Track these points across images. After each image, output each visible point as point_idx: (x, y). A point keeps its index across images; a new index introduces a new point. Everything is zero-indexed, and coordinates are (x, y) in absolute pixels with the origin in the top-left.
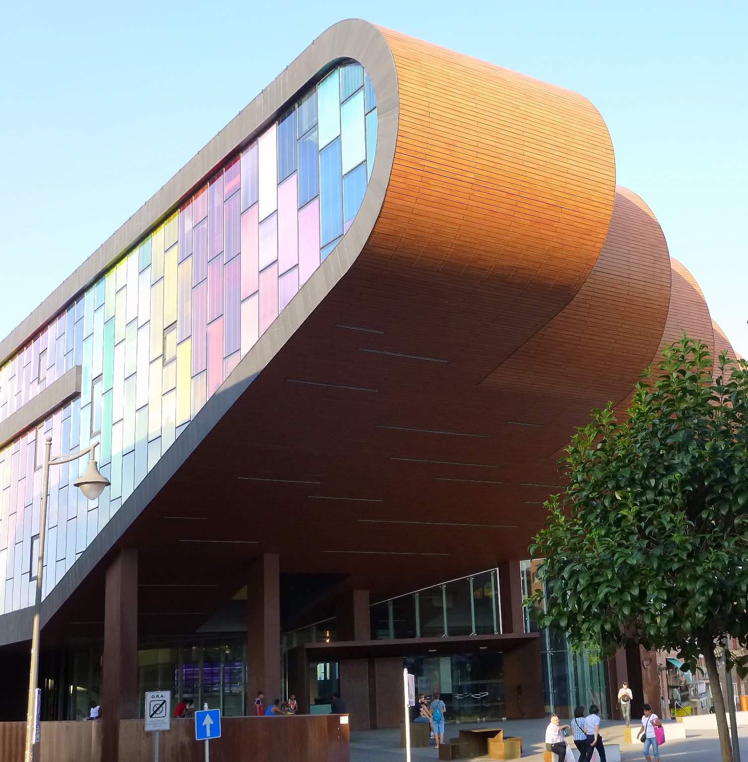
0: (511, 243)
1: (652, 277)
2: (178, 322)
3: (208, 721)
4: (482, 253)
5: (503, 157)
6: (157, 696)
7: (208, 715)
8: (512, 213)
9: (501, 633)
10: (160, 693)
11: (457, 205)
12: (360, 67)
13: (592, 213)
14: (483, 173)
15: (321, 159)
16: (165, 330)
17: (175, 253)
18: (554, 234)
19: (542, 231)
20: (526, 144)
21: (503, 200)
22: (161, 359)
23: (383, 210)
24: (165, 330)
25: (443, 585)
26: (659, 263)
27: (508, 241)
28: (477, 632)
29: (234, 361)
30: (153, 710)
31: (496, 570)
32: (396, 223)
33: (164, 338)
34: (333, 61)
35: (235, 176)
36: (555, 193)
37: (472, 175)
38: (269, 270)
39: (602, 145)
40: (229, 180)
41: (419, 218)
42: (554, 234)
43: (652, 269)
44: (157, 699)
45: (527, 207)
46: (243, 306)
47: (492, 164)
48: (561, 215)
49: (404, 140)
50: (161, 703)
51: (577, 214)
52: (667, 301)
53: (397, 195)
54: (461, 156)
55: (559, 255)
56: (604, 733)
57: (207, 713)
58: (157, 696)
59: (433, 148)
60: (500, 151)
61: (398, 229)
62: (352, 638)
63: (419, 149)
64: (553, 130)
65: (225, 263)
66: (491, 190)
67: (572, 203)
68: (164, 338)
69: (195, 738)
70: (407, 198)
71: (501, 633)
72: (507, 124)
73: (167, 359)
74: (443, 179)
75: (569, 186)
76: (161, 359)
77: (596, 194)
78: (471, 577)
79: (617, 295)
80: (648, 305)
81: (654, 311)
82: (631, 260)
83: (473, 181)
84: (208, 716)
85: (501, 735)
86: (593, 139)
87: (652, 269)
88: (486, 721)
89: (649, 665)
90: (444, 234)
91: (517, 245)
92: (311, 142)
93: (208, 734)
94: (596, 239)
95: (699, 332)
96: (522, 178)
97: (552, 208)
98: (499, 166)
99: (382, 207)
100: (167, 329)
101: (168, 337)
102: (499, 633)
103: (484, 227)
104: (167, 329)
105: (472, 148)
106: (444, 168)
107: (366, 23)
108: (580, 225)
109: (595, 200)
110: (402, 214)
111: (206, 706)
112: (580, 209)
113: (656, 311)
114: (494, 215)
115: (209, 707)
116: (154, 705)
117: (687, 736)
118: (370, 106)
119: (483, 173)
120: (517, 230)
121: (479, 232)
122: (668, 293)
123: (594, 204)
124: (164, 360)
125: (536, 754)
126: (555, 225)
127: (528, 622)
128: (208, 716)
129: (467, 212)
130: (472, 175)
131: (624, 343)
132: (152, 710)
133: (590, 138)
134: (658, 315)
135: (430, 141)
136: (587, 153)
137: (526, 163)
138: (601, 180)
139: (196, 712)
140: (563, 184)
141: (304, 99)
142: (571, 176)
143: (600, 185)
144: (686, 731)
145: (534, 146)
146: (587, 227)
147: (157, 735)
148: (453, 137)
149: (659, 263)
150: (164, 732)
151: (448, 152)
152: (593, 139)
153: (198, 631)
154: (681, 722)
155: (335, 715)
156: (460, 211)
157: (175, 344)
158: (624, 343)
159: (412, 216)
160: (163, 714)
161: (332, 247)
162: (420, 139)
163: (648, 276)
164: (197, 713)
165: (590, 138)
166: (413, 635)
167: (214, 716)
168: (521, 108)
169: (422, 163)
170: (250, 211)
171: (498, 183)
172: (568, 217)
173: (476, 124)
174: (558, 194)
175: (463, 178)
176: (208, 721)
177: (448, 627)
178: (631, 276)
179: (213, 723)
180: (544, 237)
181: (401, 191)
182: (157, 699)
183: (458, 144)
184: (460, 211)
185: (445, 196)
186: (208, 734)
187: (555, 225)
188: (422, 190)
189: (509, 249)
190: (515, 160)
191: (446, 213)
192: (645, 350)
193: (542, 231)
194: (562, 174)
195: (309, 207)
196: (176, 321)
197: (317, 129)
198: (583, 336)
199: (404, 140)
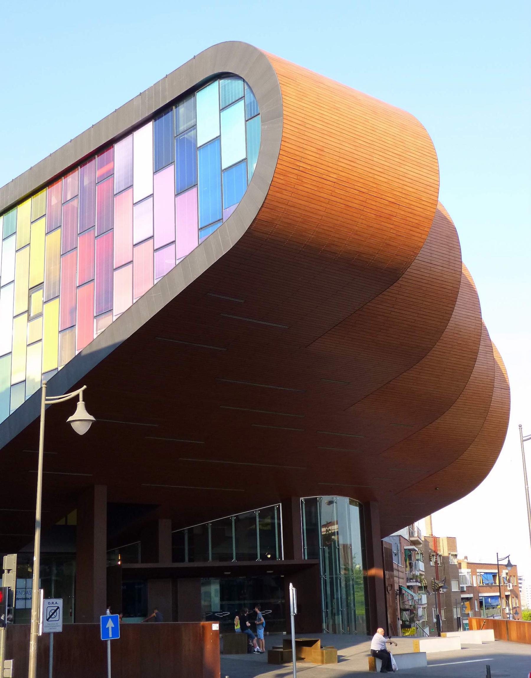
0: (358, 233)
1: (447, 263)
2: (45, 283)
3: (110, 624)
4: (335, 239)
5: (358, 162)
6: (53, 603)
7: (110, 619)
8: (362, 208)
9: (283, 559)
10: (54, 600)
11: (322, 199)
12: (240, 81)
13: (421, 210)
14: (343, 174)
15: (200, 155)
16: (30, 289)
17: (42, 224)
18: (391, 226)
19: (383, 223)
20: (375, 152)
21: (357, 197)
22: (26, 315)
23: (266, 201)
24: (30, 289)
25: (233, 517)
26: (453, 252)
27: (357, 231)
28: (261, 558)
29: (106, 321)
30: (49, 614)
31: (279, 506)
32: (274, 212)
33: (30, 297)
34: (214, 74)
35: (108, 162)
36: (395, 193)
37: (335, 176)
38: (143, 245)
39: (429, 155)
40: (101, 166)
41: (292, 209)
42: (391, 226)
43: (448, 257)
44: (53, 605)
45: (374, 203)
46: (116, 273)
47: (350, 168)
48: (398, 211)
49: (286, 144)
50: (55, 608)
51: (410, 210)
52: (458, 283)
53: (277, 189)
54: (327, 159)
55: (393, 244)
56: (389, 648)
57: (109, 617)
58: (53, 603)
59: (307, 152)
60: (356, 156)
61: (274, 217)
62: (157, 561)
63: (297, 153)
64: (394, 141)
65: (96, 236)
66: (349, 189)
67: (407, 201)
68: (30, 297)
69: (119, 639)
70: (284, 192)
71: (283, 559)
72: (362, 135)
73: (32, 315)
74: (314, 178)
75: (405, 187)
76: (26, 315)
77: (424, 194)
78: (257, 512)
79: (421, 277)
80: (444, 286)
81: (447, 291)
82: (433, 249)
83: (335, 180)
84: (110, 620)
85: (319, 643)
86: (423, 149)
87: (448, 257)
88: (270, 635)
89: (391, 590)
90: (309, 223)
91: (363, 234)
92: (189, 142)
93: (110, 636)
94: (422, 232)
95: (471, 309)
96: (371, 180)
97: (392, 205)
98: (355, 169)
99: (266, 198)
100: (32, 289)
101: (33, 296)
102: (281, 559)
103: (340, 219)
104: (32, 289)
105: (336, 153)
106: (314, 169)
107: (249, 46)
108: (411, 220)
109: (424, 199)
110: (281, 206)
111: (108, 611)
112: (412, 206)
113: (450, 292)
114: (348, 209)
115: (112, 613)
116: (50, 610)
117: (462, 648)
118: (251, 114)
119: (343, 174)
120: (364, 222)
121: (336, 222)
122: (459, 276)
123: (423, 203)
124: (29, 315)
125: (286, 667)
126: (394, 218)
127: (306, 550)
128: (110, 620)
129: (328, 206)
130: (335, 176)
131: (425, 317)
132: (58, 614)
133: (420, 148)
134: (451, 295)
135: (305, 146)
136: (419, 161)
137: (375, 168)
138: (428, 183)
139: (101, 617)
140: (401, 186)
141: (180, 104)
142: (407, 180)
143: (428, 187)
144: (462, 644)
145: (381, 154)
146: (417, 221)
147: (52, 636)
148: (321, 144)
149: (453, 252)
150: (56, 634)
151: (318, 156)
152: (423, 149)
153: (19, 551)
154: (445, 636)
155: (209, 623)
156: (323, 204)
157: (41, 303)
158: (425, 317)
159: (287, 207)
160: (57, 618)
161: (211, 230)
162: (298, 144)
163: (444, 262)
164: (102, 617)
165: (420, 148)
166: (183, 560)
167: (115, 621)
168: (370, 122)
169: (298, 163)
170: (124, 194)
171: (353, 183)
172: (403, 213)
173: (339, 134)
174: (398, 194)
175: (328, 178)
176: (110, 624)
177: (213, 554)
178: (432, 262)
179: (114, 626)
180: (384, 228)
181: (280, 186)
182: (53, 605)
183: (325, 150)
184: (323, 204)
185: (313, 192)
186: (110, 636)
187: (394, 218)
188: (296, 186)
189: (357, 237)
190: (367, 165)
191: (313, 206)
192: (439, 324)
193: (383, 223)
194: (401, 177)
195: (186, 194)
196: (43, 283)
197: (196, 128)
198: (392, 309)
199: (286, 144)
